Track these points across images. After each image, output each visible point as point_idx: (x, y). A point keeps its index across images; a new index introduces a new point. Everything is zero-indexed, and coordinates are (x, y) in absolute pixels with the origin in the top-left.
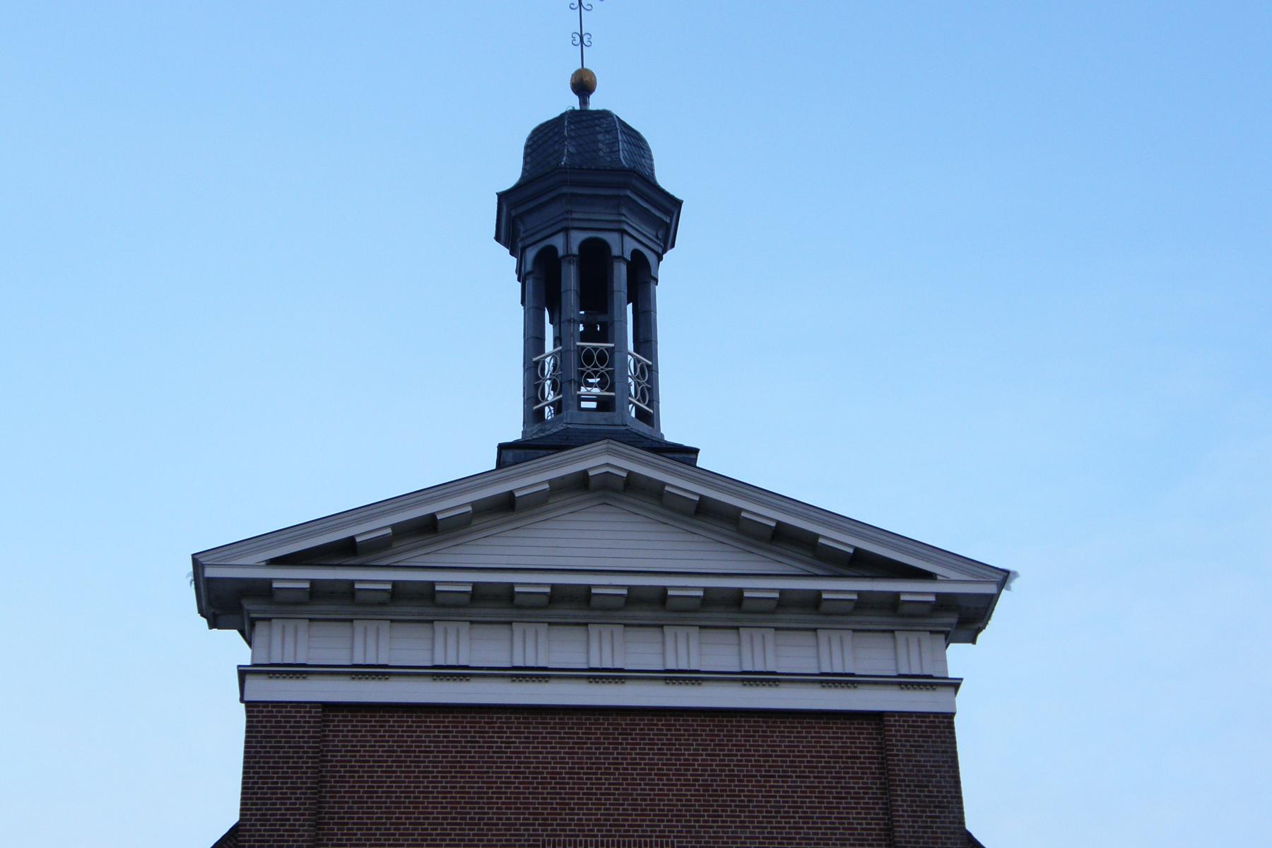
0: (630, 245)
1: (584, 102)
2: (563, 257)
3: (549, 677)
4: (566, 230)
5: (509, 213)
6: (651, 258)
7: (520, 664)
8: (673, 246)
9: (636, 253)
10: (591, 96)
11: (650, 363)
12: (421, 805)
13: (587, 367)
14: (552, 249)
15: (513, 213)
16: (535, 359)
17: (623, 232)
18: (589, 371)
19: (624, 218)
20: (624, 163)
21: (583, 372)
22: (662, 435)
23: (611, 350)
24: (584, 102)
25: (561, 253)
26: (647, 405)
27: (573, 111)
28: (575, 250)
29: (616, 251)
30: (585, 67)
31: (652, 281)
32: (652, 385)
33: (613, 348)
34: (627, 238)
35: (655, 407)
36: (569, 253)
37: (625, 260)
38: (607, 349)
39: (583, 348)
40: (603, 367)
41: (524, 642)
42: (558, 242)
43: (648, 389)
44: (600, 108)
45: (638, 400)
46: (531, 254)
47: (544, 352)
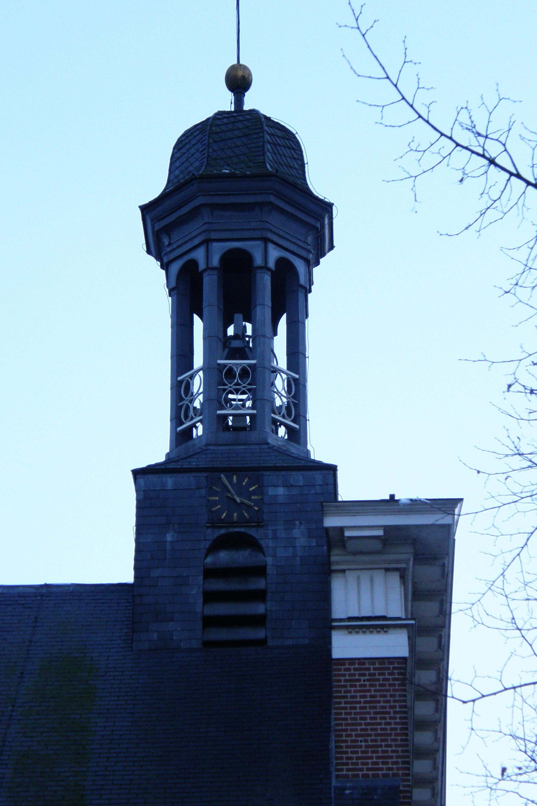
0: (274, 254)
1: (239, 101)
2: (204, 270)
3: (388, 626)
4: (207, 242)
5: (153, 226)
6: (300, 266)
7: (355, 614)
8: (332, 247)
9: (282, 262)
10: (246, 94)
11: (297, 376)
12: (397, 698)
13: (230, 385)
14: (193, 263)
15: (157, 227)
16: (219, 362)
17: (266, 240)
18: (230, 385)
19: (268, 226)
20: (270, 169)
21: (224, 390)
22: (308, 452)
23: (253, 367)
24: (239, 101)
25: (202, 266)
26: (294, 421)
27: (220, 115)
28: (215, 261)
29: (258, 260)
30: (241, 62)
31: (300, 289)
32: (299, 402)
33: (255, 364)
34: (271, 246)
35: (301, 423)
36: (210, 266)
37: (269, 269)
38: (250, 365)
39: (225, 365)
40: (231, 385)
41: (359, 592)
42: (199, 255)
43: (295, 404)
44: (251, 108)
45: (283, 417)
46: (176, 267)
47: (192, 367)
